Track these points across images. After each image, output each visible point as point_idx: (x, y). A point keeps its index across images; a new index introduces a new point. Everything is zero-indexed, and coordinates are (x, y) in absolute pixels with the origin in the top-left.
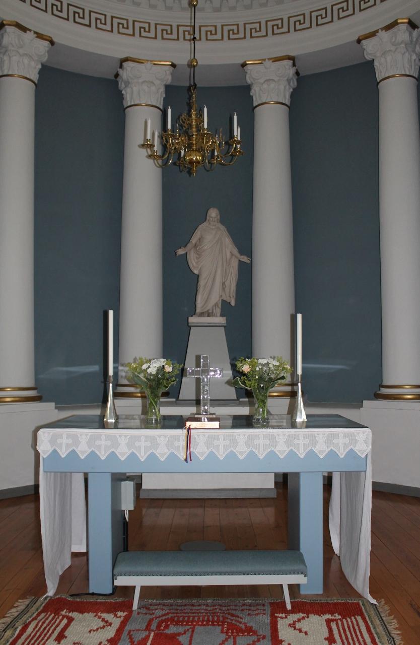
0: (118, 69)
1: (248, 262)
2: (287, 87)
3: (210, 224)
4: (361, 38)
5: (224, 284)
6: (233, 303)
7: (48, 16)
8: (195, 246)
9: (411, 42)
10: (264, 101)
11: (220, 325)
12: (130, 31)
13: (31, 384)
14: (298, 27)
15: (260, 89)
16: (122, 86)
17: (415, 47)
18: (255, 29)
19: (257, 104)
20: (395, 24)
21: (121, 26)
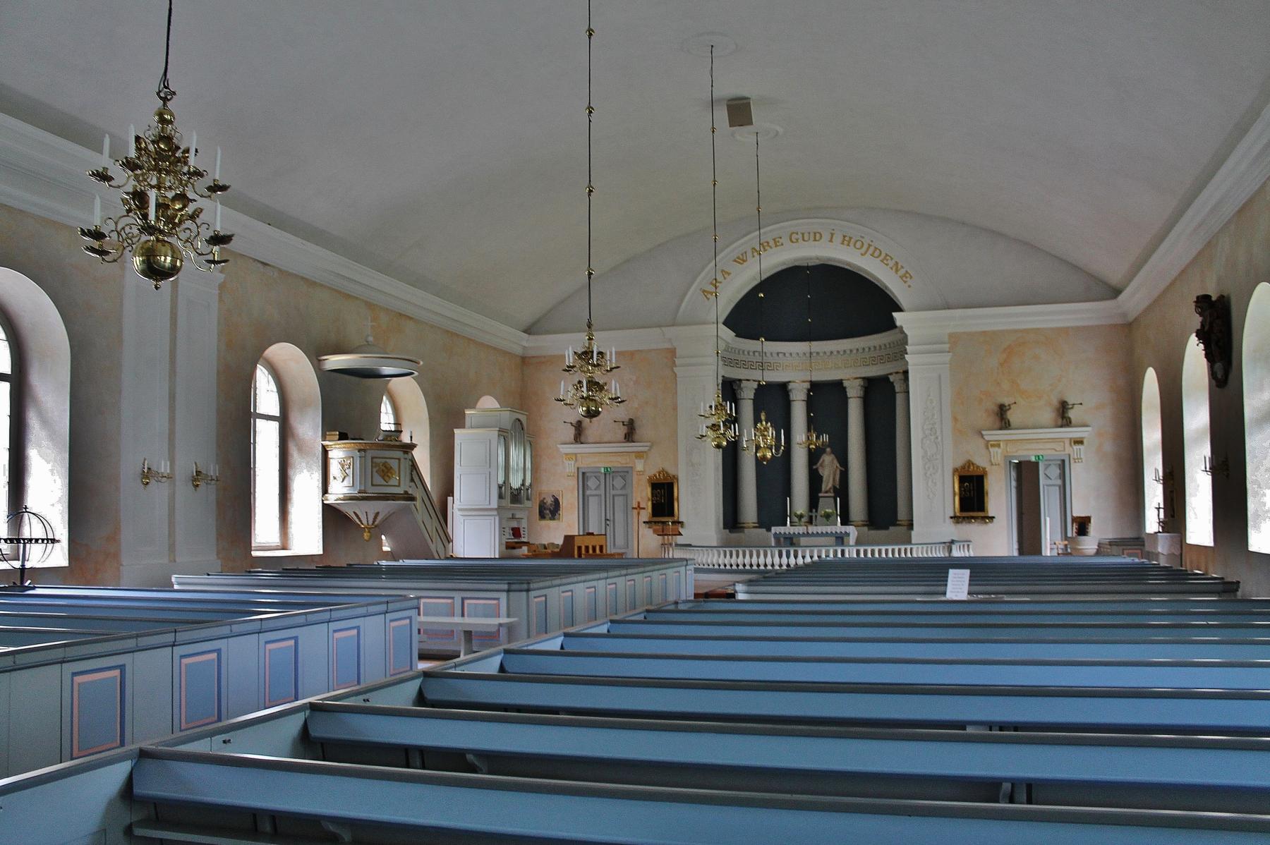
6: (838, 487)
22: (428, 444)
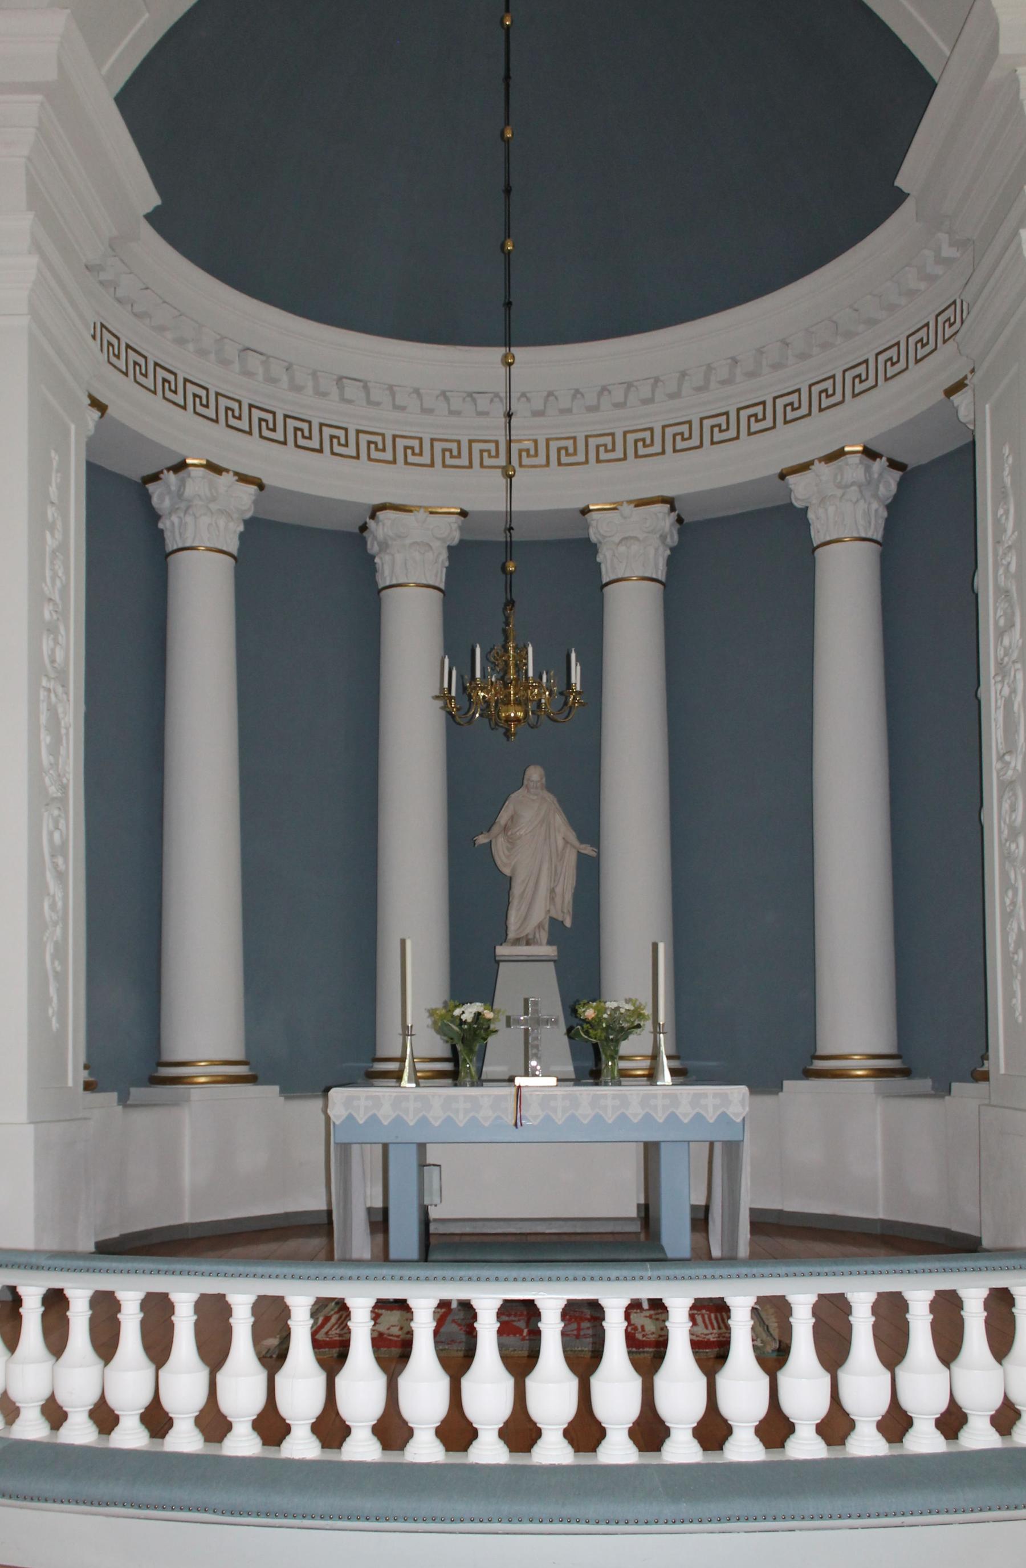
0: (368, 520)
1: (594, 854)
2: (661, 549)
4: (784, 472)
5: (552, 891)
6: (568, 923)
7: (253, 443)
8: (505, 829)
9: (869, 483)
10: (620, 576)
11: (548, 958)
12: (388, 455)
13: (240, 1056)
14: (680, 445)
16: (373, 547)
17: (877, 488)
18: (605, 446)
19: (608, 580)
20: (839, 454)
21: (372, 446)
22: (214, 474)
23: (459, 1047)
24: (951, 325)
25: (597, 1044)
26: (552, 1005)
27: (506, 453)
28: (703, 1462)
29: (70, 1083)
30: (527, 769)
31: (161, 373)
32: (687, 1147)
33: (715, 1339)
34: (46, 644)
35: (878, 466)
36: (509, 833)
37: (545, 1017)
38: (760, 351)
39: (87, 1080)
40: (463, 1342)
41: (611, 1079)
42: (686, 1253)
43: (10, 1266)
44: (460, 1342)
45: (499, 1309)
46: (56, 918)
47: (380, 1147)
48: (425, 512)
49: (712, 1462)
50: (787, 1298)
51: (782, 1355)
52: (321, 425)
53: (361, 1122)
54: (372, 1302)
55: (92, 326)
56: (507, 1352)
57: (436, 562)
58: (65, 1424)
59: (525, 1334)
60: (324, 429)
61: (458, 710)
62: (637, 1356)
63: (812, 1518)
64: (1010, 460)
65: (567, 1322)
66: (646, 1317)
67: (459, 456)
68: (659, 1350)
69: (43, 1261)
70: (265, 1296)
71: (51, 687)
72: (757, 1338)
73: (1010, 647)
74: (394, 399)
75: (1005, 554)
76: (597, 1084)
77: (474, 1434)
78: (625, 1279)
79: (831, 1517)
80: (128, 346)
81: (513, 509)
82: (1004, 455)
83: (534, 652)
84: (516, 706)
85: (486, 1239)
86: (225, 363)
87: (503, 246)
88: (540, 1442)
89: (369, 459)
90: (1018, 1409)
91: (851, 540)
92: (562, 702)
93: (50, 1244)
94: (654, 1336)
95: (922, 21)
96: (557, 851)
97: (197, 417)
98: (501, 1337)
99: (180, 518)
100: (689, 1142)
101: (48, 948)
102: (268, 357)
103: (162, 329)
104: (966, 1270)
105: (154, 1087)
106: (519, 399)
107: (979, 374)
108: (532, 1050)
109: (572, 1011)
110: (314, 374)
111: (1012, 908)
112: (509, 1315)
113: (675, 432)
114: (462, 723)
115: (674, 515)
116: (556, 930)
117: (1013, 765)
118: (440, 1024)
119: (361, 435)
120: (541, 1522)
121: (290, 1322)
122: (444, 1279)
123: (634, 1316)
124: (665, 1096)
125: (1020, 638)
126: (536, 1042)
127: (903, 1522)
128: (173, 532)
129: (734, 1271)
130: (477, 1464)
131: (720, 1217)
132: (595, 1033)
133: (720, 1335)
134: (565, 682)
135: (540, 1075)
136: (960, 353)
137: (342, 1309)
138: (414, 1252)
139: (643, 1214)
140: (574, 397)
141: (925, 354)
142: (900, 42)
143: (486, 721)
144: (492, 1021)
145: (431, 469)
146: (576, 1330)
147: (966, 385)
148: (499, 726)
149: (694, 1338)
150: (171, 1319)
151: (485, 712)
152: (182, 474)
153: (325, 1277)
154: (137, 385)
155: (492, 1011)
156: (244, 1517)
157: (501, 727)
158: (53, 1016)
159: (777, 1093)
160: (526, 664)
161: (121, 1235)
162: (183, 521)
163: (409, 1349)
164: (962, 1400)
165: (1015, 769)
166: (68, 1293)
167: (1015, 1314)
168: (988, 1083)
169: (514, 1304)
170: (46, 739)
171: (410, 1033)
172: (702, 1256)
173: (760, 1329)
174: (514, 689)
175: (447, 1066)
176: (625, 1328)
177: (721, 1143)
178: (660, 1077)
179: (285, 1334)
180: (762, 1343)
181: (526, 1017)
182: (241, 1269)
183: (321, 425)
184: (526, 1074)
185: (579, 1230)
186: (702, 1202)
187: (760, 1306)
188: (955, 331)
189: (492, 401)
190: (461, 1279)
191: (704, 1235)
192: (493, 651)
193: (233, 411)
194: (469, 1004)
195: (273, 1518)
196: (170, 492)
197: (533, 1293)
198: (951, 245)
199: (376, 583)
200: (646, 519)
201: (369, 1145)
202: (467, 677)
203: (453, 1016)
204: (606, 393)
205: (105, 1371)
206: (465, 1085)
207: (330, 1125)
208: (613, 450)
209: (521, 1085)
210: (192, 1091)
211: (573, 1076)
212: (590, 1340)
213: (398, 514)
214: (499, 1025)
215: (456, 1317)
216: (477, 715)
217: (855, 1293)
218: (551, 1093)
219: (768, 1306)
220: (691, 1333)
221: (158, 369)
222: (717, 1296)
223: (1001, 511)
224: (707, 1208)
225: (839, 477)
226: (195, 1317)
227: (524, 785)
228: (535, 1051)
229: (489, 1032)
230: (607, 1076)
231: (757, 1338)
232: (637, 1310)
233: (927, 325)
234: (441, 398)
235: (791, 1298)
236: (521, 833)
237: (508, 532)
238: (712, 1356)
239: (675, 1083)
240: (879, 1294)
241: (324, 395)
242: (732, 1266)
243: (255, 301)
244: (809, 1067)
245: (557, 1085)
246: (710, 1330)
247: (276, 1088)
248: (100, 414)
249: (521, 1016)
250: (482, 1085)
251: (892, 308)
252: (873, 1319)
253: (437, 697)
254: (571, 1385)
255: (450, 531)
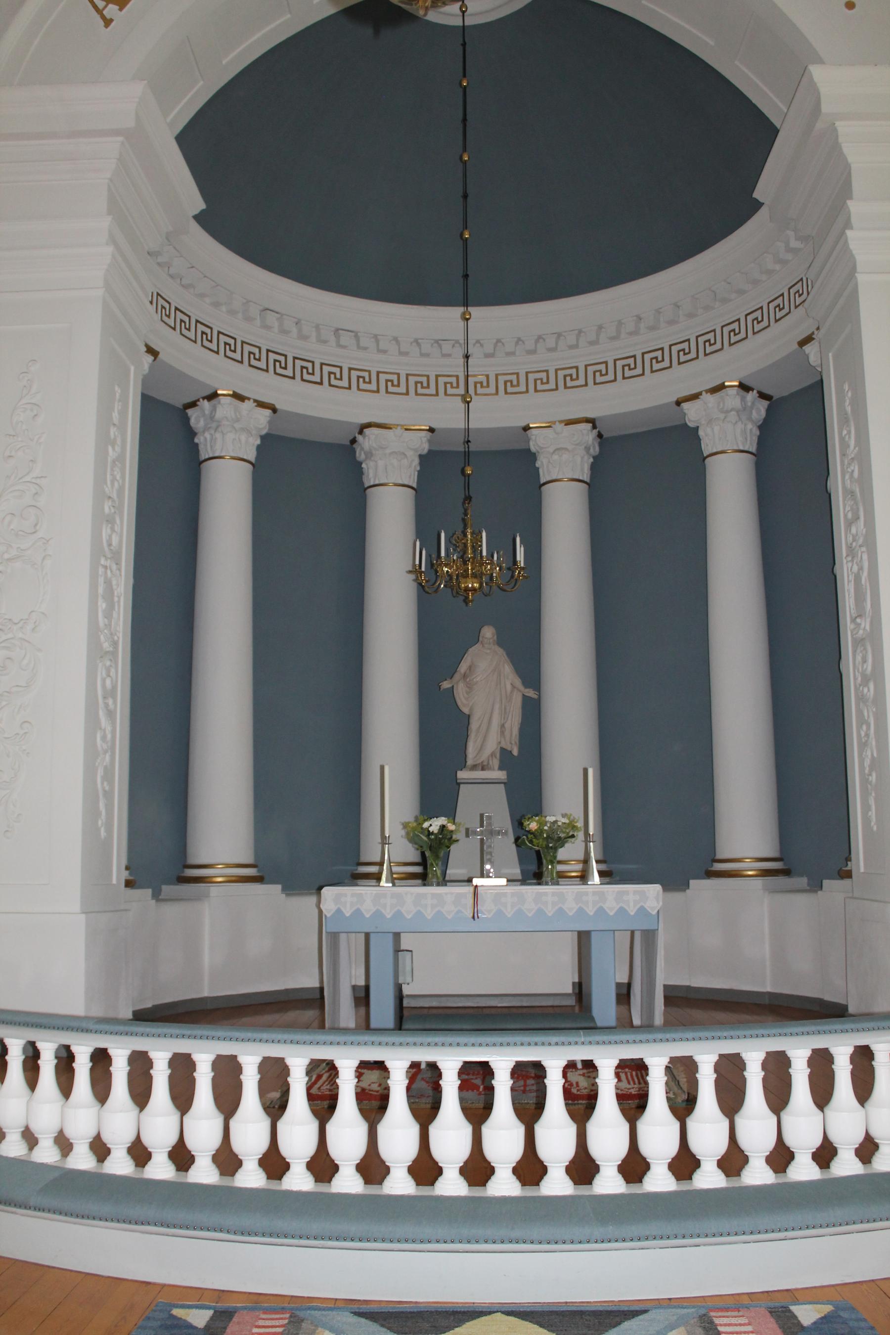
0: (357, 435)
1: (536, 697)
2: (586, 457)
3: (483, 646)
4: (680, 400)
5: (503, 726)
6: (515, 752)
7: (270, 378)
8: (465, 676)
9: (744, 409)
10: (554, 477)
12: (373, 387)
15: (549, 462)
16: (360, 456)
18: (541, 379)
19: (545, 481)
20: (721, 387)
21: (361, 380)
22: (239, 402)
23: (428, 854)
24: (800, 296)
25: (539, 851)
26: (502, 819)
27: (465, 385)
28: (626, 1193)
29: (114, 881)
30: (482, 629)
31: (201, 328)
32: (612, 935)
33: (636, 1093)
34: (105, 532)
35: (751, 396)
36: (468, 680)
37: (497, 829)
38: (658, 311)
39: (127, 878)
40: (430, 1096)
41: (551, 880)
42: (613, 1022)
43: (65, 1029)
44: (428, 1097)
45: (460, 1069)
46: (106, 747)
47: (362, 936)
48: (401, 429)
49: (633, 1192)
50: (694, 1058)
51: (691, 1105)
52: (322, 364)
53: (348, 915)
54: (356, 1063)
55: (151, 294)
56: (466, 1105)
57: (410, 467)
58: (109, 1158)
59: (481, 1089)
60: (324, 367)
61: (427, 581)
62: (572, 1107)
63: (714, 1235)
64: (850, 394)
65: (515, 1080)
66: (580, 1075)
67: (428, 387)
68: (590, 1102)
69: (91, 1026)
70: (269, 1057)
71: (108, 565)
72: (670, 1091)
73: (857, 535)
74: (378, 345)
75: (849, 464)
76: (539, 884)
77: (439, 1171)
78: (563, 1044)
79: (729, 1234)
80: (176, 309)
81: (470, 427)
82: (845, 390)
83: (487, 536)
84: (473, 579)
85: (449, 1012)
86: (249, 319)
87: (462, 235)
88: (493, 1178)
89: (358, 389)
90: (876, 1143)
91: (732, 452)
92: (510, 575)
93: (97, 1011)
94: (586, 1090)
95: (765, 88)
96: (506, 695)
97: (226, 359)
98: (461, 1092)
99: (211, 434)
100: (614, 931)
101: (99, 771)
102: (282, 315)
103: (202, 296)
104: (836, 1032)
105: (181, 885)
106: (474, 345)
107: (822, 331)
108: (486, 856)
109: (519, 824)
110: (317, 327)
111: (866, 739)
112: (468, 1074)
113: (594, 370)
114: (430, 592)
115: (595, 432)
116: (505, 758)
117: (863, 626)
118: (412, 835)
119: (352, 372)
120: (494, 1243)
121: (289, 1079)
122: (415, 1044)
123: (570, 1074)
124: (594, 893)
125: (864, 528)
126: (489, 850)
127: (786, 1236)
128: (206, 445)
129: (651, 1037)
130: (442, 1196)
131: (640, 993)
132: (537, 841)
133: (640, 1089)
134: (512, 559)
135: (493, 877)
136: (808, 316)
137: (332, 1068)
138: (390, 1022)
139: (577, 991)
140: (517, 343)
141: (782, 316)
142: (751, 102)
143: (450, 590)
144: (454, 832)
145: (406, 396)
146: (522, 1086)
147: (814, 339)
148: (459, 594)
149: (619, 1092)
150: (193, 1075)
151: (448, 583)
152: (214, 402)
153: (318, 1043)
154: (182, 337)
155: (454, 824)
156: (252, 1236)
157: (461, 595)
158: (102, 826)
159: (684, 890)
160: (481, 546)
161: (153, 1006)
162: (214, 437)
163: (386, 1102)
164: (834, 1137)
165: (864, 629)
166: (111, 1052)
167: (874, 1066)
168: (851, 879)
169: (472, 1065)
170: (102, 605)
171: (387, 842)
172: (625, 1024)
173: (672, 1084)
174: (471, 565)
175: (418, 869)
176: (563, 1084)
177: (640, 931)
178: (591, 878)
179: (285, 1089)
180: (674, 1095)
181: (481, 829)
182: (249, 1035)
183: (322, 364)
184: (482, 876)
185: (525, 1004)
186: (625, 980)
187: (672, 1065)
188: (803, 300)
189: (453, 346)
190: (429, 1044)
191: (627, 1007)
192: (455, 536)
193: (254, 354)
194: (435, 818)
195: (275, 1238)
196: (204, 415)
197: (488, 1056)
198: (796, 239)
199: (363, 484)
200: (574, 435)
201: (354, 934)
202: (434, 556)
203: (422, 828)
204: (541, 340)
205: (140, 1115)
206: (432, 885)
207: (322, 917)
208: (548, 382)
209: (478, 885)
210: (212, 888)
211: (520, 877)
212: (535, 1094)
213: (381, 430)
214: (460, 835)
215: (424, 1076)
216: (442, 586)
217: (749, 1053)
218: (502, 891)
219: (679, 1065)
220: (617, 1088)
221: (198, 325)
222: (638, 1057)
223: (845, 432)
224: (629, 985)
225: (721, 405)
226: (212, 1074)
227: (480, 642)
228: (489, 857)
229: (452, 841)
230: (548, 877)
231: (670, 1091)
232: (572, 1069)
233: (782, 295)
234: (414, 344)
235: (697, 1058)
236: (477, 680)
237: (466, 444)
238: (634, 1106)
239: (602, 883)
240: (767, 1053)
241: (325, 342)
242: (650, 1032)
243: (273, 275)
244: (710, 869)
245: (507, 885)
246: (632, 1085)
247: (279, 887)
248: (153, 358)
249: (478, 828)
250: (446, 885)
251: (756, 282)
252: (763, 1073)
253: (410, 572)
254: (518, 1131)
255: (421, 443)
